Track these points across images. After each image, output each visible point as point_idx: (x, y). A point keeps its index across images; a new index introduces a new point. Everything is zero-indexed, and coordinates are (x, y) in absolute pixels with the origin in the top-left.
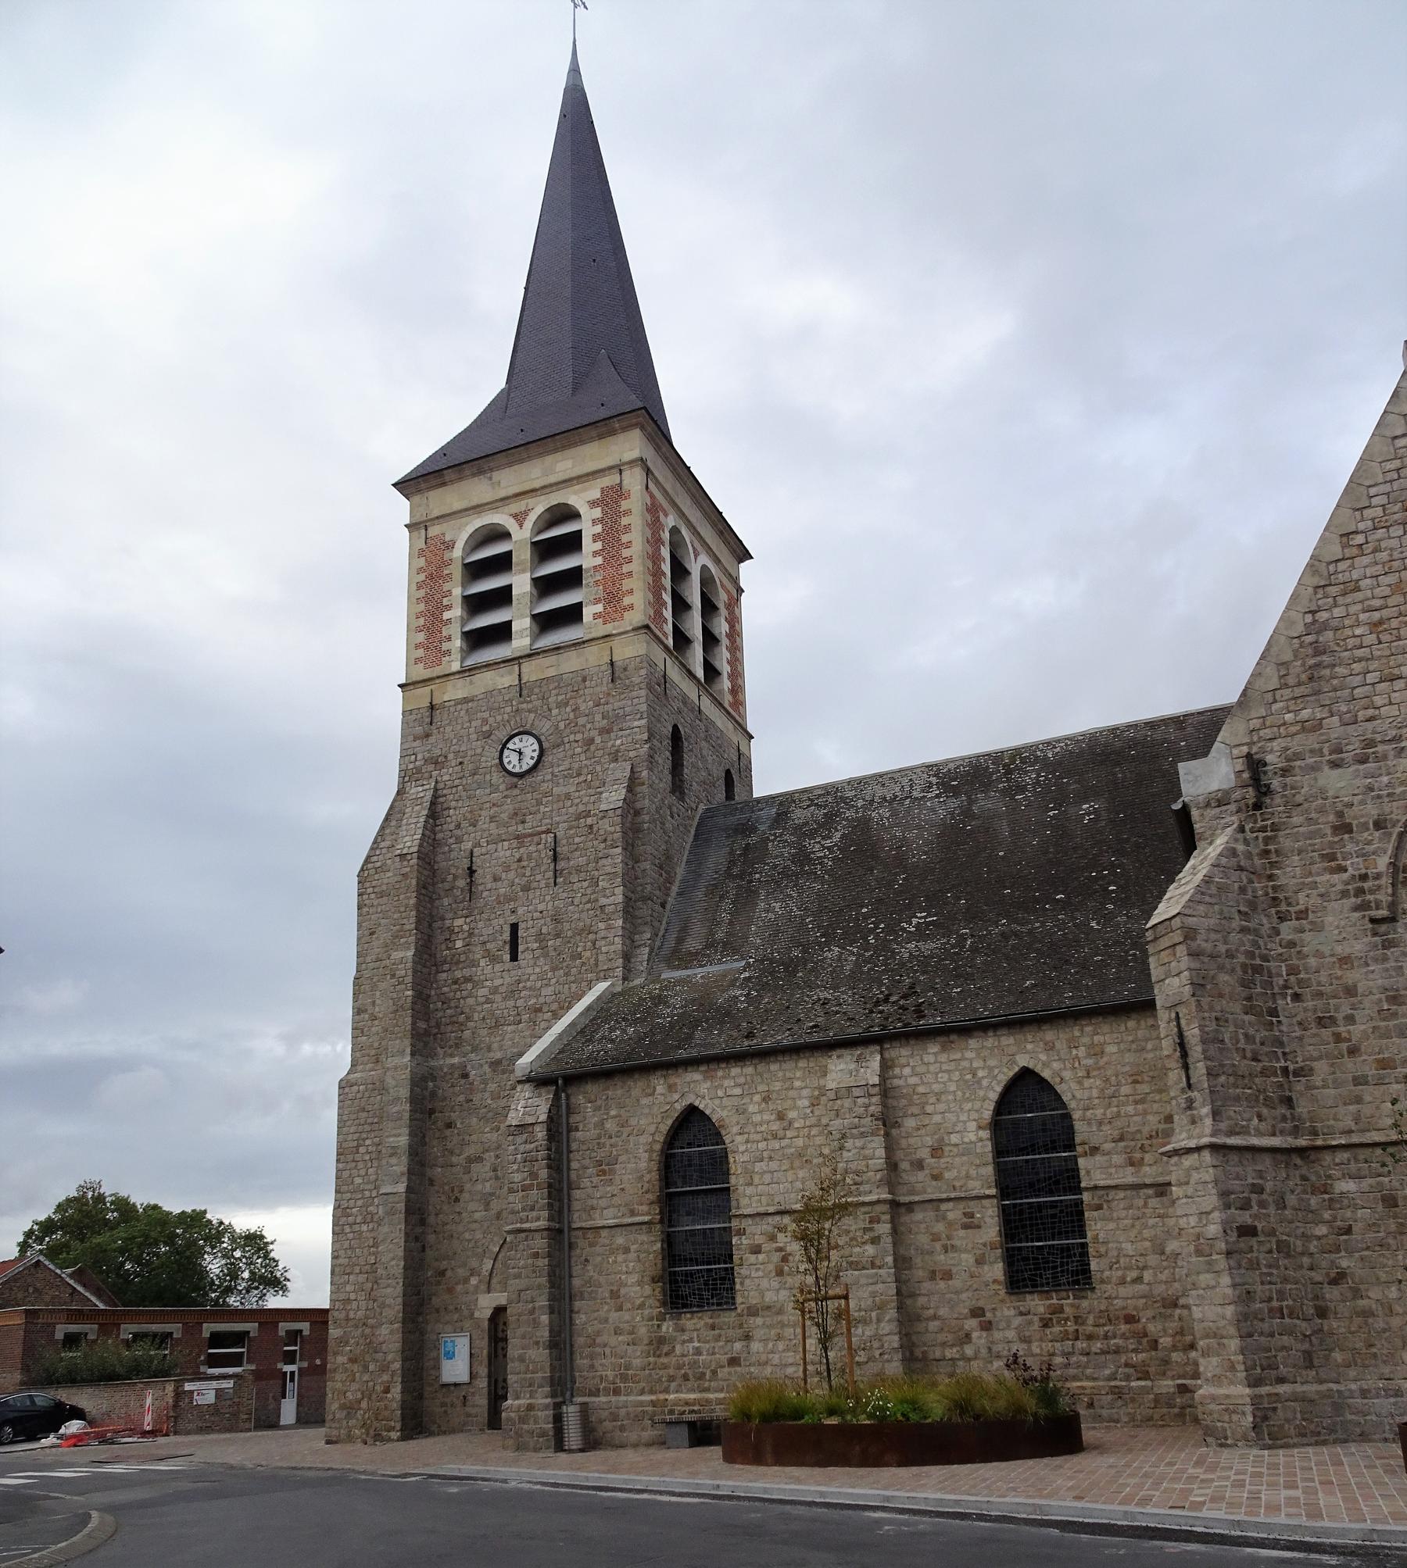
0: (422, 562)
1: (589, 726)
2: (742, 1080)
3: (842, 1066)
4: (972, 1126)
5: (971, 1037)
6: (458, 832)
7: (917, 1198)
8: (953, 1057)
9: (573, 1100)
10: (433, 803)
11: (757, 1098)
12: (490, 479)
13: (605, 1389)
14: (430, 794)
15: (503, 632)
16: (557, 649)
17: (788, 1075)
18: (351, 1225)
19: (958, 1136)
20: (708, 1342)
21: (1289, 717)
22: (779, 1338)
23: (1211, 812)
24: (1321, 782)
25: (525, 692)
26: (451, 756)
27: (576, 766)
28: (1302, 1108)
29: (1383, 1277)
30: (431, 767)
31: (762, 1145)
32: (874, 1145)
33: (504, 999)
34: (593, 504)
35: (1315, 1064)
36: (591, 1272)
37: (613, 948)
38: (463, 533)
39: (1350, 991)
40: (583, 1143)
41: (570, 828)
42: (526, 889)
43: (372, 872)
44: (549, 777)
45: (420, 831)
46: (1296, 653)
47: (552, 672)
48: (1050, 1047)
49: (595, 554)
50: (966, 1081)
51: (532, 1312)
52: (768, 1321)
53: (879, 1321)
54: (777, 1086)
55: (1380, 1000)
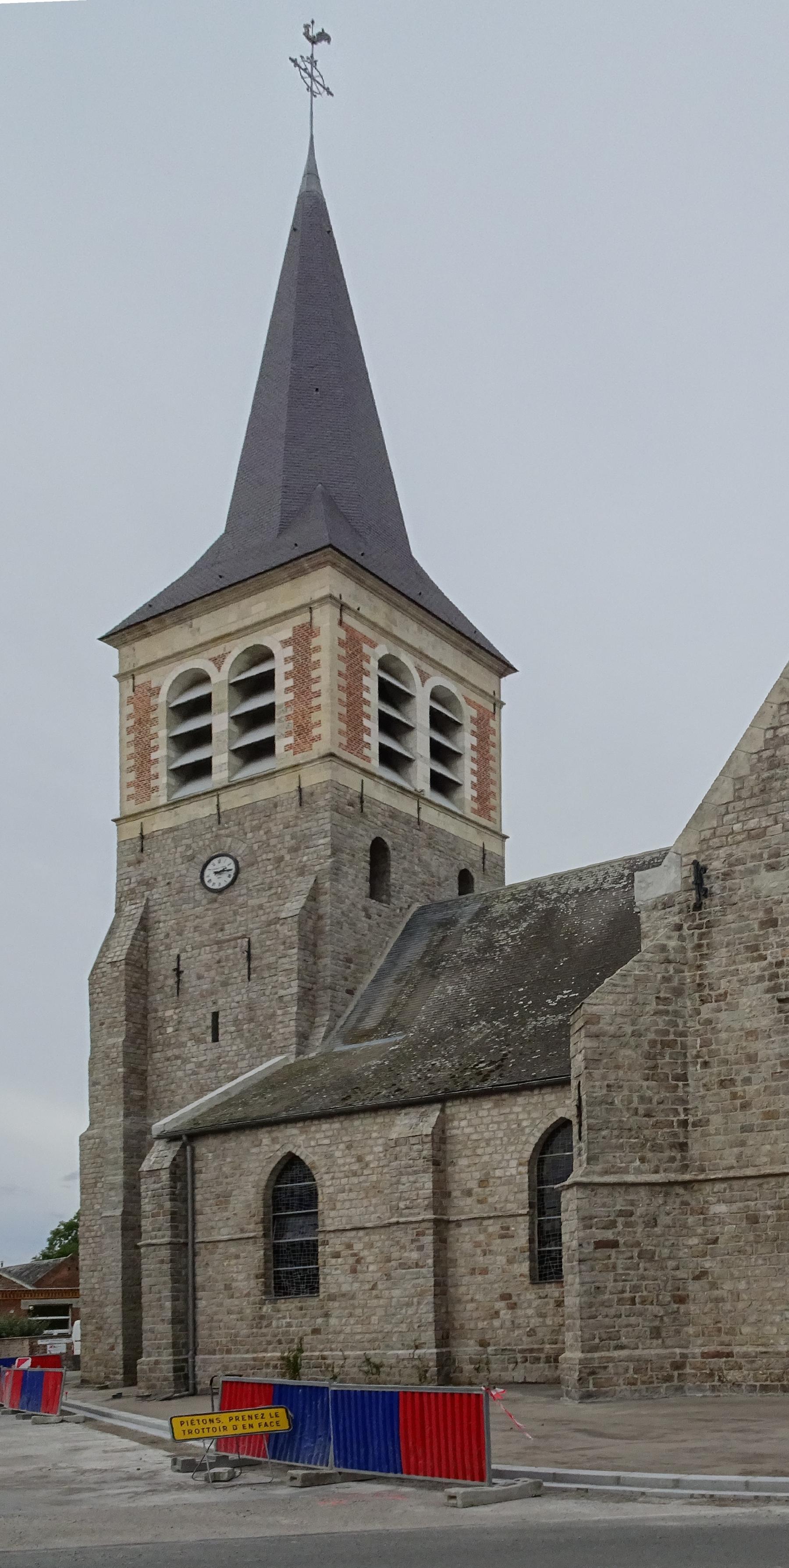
0: (130, 709)
1: (279, 846)
2: (330, 1133)
3: (406, 1121)
4: (514, 1163)
5: (519, 1096)
6: (167, 941)
7: (463, 1217)
8: (502, 1111)
9: (197, 1151)
10: (142, 919)
11: (342, 1146)
12: (191, 626)
13: (220, 1350)
14: (141, 910)
15: (203, 768)
16: (251, 780)
17: (368, 1128)
18: (93, 1237)
19: (502, 1171)
20: (297, 1318)
21: (737, 827)
22: (351, 1315)
23: (656, 914)
24: (756, 884)
25: (223, 820)
26: (160, 878)
27: (268, 881)
28: (695, 1150)
29: (736, 1274)
30: (143, 888)
31: (344, 1181)
32: (423, 1180)
33: (208, 1071)
34: (285, 643)
35: (711, 1117)
37: (288, 1030)
38: (165, 680)
39: (751, 1058)
40: (206, 1182)
41: (262, 934)
42: (225, 984)
43: (100, 975)
44: (244, 891)
45: (129, 942)
46: (753, 768)
47: (247, 801)
49: (287, 690)
50: (512, 1130)
51: (159, 1299)
52: (344, 1304)
53: (419, 1303)
54: (359, 1136)
55: (775, 1065)
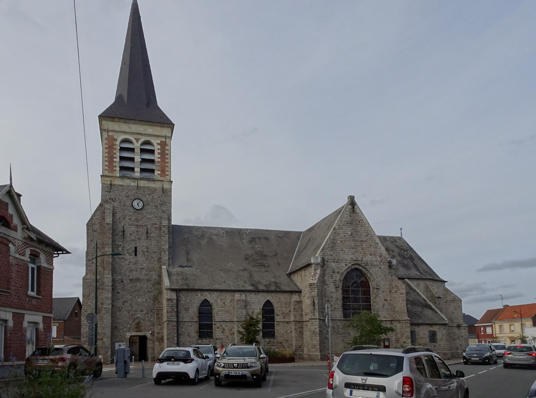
30: (111, 201)
34: (158, 144)
36: (183, 330)
48: (273, 296)
